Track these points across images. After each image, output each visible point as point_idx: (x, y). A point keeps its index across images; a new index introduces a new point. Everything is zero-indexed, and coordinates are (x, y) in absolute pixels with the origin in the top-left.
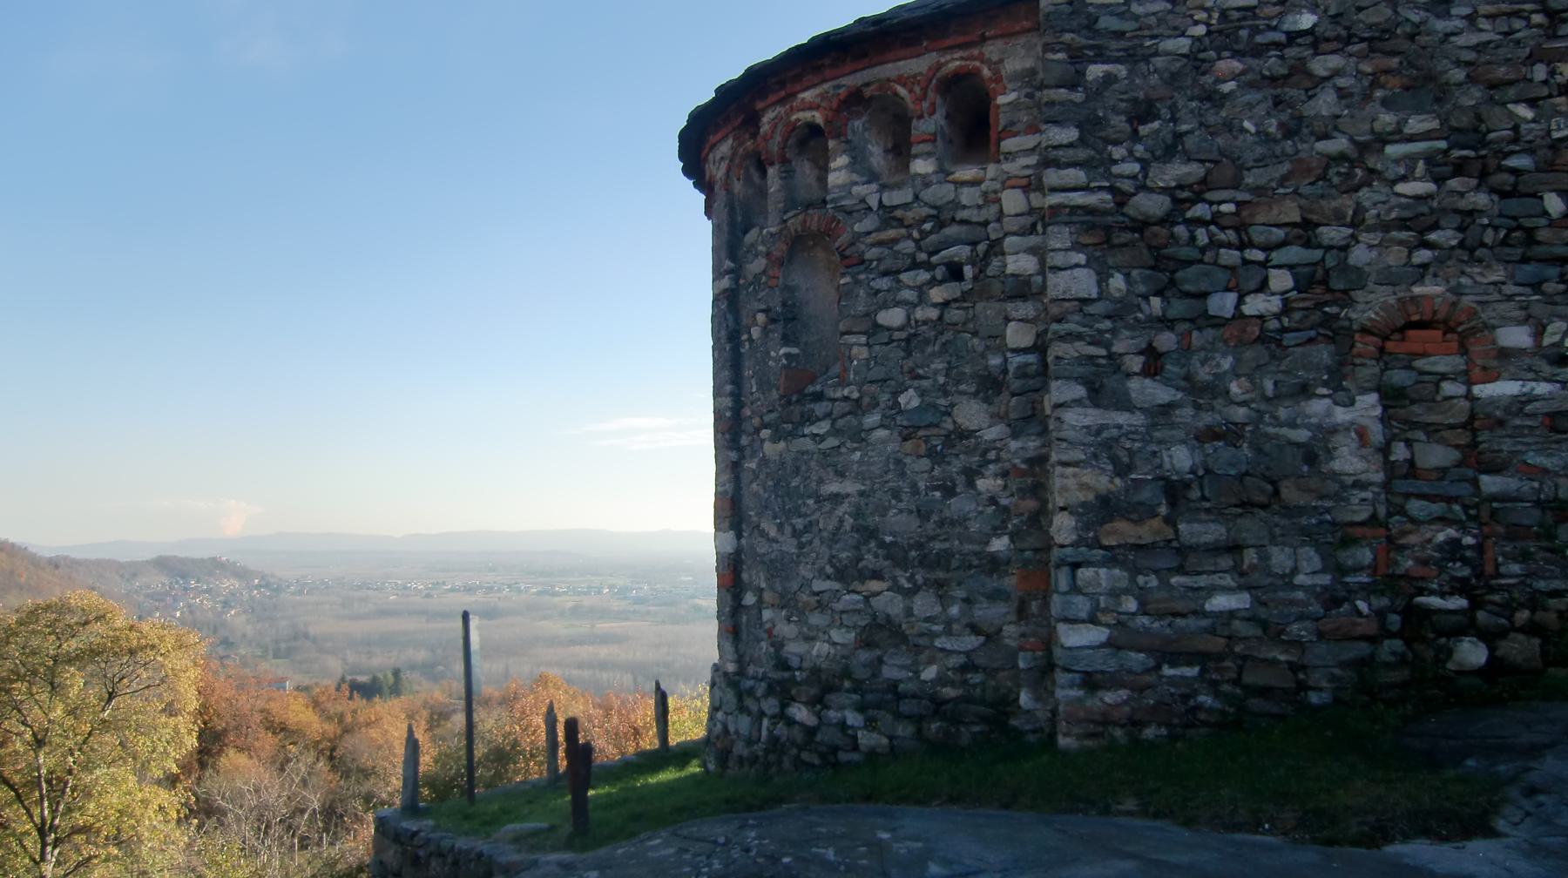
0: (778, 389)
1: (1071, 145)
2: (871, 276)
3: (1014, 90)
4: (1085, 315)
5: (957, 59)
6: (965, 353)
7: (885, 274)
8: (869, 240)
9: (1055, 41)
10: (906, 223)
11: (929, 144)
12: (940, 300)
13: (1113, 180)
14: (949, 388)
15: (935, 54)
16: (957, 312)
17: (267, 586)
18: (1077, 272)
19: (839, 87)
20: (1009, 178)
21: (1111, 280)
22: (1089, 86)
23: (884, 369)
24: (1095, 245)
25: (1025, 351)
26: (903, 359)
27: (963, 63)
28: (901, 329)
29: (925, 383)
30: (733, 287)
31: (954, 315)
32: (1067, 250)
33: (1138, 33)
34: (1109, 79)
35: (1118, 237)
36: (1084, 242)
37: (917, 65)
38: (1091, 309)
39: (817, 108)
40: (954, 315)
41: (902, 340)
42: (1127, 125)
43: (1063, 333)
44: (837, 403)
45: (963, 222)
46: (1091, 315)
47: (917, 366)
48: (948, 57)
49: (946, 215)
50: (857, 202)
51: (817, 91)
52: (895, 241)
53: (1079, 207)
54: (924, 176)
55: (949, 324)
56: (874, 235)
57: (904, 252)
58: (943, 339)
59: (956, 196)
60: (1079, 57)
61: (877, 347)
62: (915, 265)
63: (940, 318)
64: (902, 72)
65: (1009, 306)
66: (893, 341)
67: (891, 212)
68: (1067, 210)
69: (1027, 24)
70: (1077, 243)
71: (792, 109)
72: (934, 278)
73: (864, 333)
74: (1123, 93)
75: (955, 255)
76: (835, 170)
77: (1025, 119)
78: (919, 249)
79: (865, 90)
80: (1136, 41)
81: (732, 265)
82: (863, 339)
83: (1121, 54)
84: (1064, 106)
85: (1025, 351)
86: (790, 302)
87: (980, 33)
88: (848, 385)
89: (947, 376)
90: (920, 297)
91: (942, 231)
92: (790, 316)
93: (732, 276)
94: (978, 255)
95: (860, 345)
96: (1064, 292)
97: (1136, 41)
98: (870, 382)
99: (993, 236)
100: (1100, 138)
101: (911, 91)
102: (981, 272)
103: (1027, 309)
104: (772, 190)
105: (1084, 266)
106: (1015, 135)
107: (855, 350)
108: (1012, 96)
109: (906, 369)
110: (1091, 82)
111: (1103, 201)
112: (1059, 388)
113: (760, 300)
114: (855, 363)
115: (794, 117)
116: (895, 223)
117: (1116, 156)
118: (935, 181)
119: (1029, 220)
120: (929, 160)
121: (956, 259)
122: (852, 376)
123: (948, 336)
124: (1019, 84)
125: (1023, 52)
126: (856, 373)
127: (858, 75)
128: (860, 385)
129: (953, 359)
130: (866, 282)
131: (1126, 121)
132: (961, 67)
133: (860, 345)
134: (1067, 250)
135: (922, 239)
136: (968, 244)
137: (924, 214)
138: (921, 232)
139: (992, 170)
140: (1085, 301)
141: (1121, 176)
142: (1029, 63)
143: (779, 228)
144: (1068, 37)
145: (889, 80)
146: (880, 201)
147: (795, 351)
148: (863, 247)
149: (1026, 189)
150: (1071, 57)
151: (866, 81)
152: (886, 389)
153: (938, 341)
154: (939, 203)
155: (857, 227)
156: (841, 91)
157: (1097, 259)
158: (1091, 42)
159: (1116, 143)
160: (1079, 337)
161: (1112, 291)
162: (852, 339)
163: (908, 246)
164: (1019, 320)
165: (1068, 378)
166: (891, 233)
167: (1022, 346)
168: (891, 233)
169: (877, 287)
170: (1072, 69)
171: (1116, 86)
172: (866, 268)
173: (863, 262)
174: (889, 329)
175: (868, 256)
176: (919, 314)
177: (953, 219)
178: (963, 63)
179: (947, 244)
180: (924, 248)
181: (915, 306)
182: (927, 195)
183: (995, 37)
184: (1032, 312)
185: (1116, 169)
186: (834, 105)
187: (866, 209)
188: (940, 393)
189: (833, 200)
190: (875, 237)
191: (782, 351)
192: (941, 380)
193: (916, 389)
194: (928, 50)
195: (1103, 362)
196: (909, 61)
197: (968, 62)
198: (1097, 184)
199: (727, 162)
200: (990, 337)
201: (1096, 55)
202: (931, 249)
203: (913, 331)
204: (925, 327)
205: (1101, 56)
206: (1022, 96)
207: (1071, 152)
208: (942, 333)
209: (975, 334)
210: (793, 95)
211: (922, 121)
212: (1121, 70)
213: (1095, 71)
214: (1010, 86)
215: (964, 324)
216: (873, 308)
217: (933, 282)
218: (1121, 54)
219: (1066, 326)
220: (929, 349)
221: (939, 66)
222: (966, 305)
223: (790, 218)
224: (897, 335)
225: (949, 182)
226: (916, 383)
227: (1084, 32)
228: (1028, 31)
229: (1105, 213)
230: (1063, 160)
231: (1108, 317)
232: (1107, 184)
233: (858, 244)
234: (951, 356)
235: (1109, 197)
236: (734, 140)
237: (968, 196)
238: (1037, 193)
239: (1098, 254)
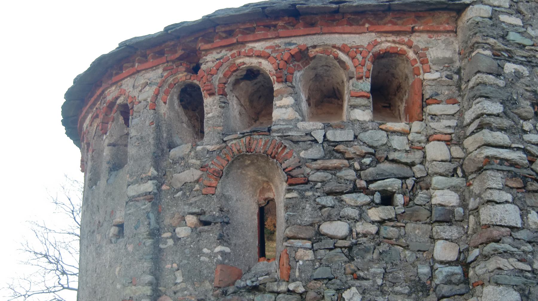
0: (212, 281)
1: (498, 115)
2: (318, 194)
3: (437, 71)
4: (514, 239)
5: (389, 42)
6: (399, 262)
7: (329, 194)
8: (315, 165)
9: (484, 41)
10: (347, 156)
11: (365, 99)
12: (377, 219)
13: (526, 144)
14: (385, 288)
15: (374, 34)
16: (392, 229)
18: (507, 206)
19: (290, 44)
20: (435, 133)
21: (529, 215)
22: (507, 77)
23: (328, 269)
24: (518, 188)
25: (449, 263)
26: (346, 262)
27: (393, 45)
28: (344, 238)
29: (365, 283)
30: (156, 191)
31: (389, 231)
32: (499, 189)
33: (533, 48)
34: (518, 75)
35: (531, 185)
36: (510, 185)
38: (518, 235)
39: (267, 57)
40: (389, 231)
41: (345, 247)
42: (531, 108)
43: (501, 251)
44: (280, 295)
45: (394, 161)
46: (519, 239)
47: (359, 269)
48: (383, 39)
49: (381, 154)
50: (304, 134)
52: (338, 169)
53: (507, 160)
54: (362, 123)
55: (384, 238)
56: (319, 162)
57: (346, 178)
58: (381, 249)
59: (389, 140)
60: (499, 56)
61: (322, 252)
62: (355, 190)
63: (378, 233)
64: (346, 43)
65: (437, 228)
66: (335, 247)
67: (335, 146)
68: (498, 161)
69: (448, 27)
70: (506, 185)
71: (239, 54)
72: (373, 201)
73: (309, 239)
74: (527, 86)
75: (390, 186)
76: (281, 107)
77: (447, 92)
78: (359, 177)
79: (310, 50)
80: (532, 53)
81: (156, 173)
82: (308, 244)
83: (524, 59)
84: (492, 87)
85: (449, 263)
86: (225, 209)
87: (412, 26)
88: (294, 281)
89: (383, 278)
90: (360, 215)
91: (378, 165)
92: (226, 220)
93: (155, 181)
94: (407, 188)
95: (306, 249)
96: (501, 220)
97: (532, 53)
98: (315, 280)
99: (418, 175)
100: (516, 113)
101: (353, 58)
102: (410, 200)
103: (452, 231)
104: (210, 115)
105: (511, 203)
106: (438, 103)
107: (300, 252)
108: (436, 75)
109: (348, 270)
110: (507, 74)
111: (521, 158)
112: (501, 292)
113: (191, 204)
114: (301, 262)
115: (239, 61)
116: (338, 155)
117: (526, 128)
118: (370, 128)
119: (453, 166)
120: (367, 111)
121: (389, 188)
122: (297, 274)
123: (384, 247)
124: (442, 68)
125: (443, 46)
126: (301, 272)
127: (309, 38)
128: (306, 282)
129: (389, 266)
130: (313, 198)
131: (530, 105)
132: (391, 48)
133: (306, 249)
134: (499, 189)
135: (362, 169)
136: (399, 178)
137: (364, 151)
138: (361, 164)
139: (416, 126)
140: (512, 228)
141: (529, 142)
142: (448, 54)
143: (218, 146)
144: (491, 41)
145: (334, 47)
146: (325, 136)
147: (227, 250)
148: (308, 170)
149: (448, 143)
150: (494, 55)
151: (315, 44)
152: (331, 286)
153: (376, 251)
154: (375, 144)
155: (302, 154)
156: (292, 47)
157: (519, 199)
158: (506, 47)
159: (526, 119)
160: (512, 255)
161: (530, 223)
162: (297, 243)
163: (350, 174)
164: (446, 240)
165: (507, 285)
166: (335, 162)
167: (449, 259)
168: (335, 162)
169: (323, 203)
170: (495, 63)
171: (522, 80)
172: (311, 188)
173: (307, 182)
174: (332, 237)
175: (312, 178)
176: (360, 228)
177: (387, 158)
178: (393, 45)
179: (383, 177)
180: (363, 177)
181: (357, 221)
182: (365, 136)
183: (421, 32)
184: (456, 234)
185: (526, 137)
186: (286, 56)
187: (312, 141)
188: (379, 292)
189: (278, 131)
190: (320, 164)
191: (219, 249)
192: (379, 282)
193: (358, 287)
194: (369, 31)
195: (529, 275)
196: (352, 35)
197: (397, 45)
198: (516, 146)
199: (154, 88)
200: (419, 251)
201: (509, 57)
202: (370, 178)
203: (354, 241)
204: (365, 239)
205: (510, 59)
206: (444, 76)
207: (499, 120)
208: (379, 245)
209: (406, 247)
210: (243, 43)
211: (361, 81)
212: (525, 70)
213: (510, 68)
214: (434, 67)
215: (398, 239)
216: (318, 220)
217: (372, 204)
218: (524, 59)
219: (503, 245)
220: (369, 257)
221: (376, 43)
222: (399, 224)
223: (231, 140)
224: (341, 243)
225: (382, 129)
226: (357, 283)
227: (501, 39)
228: (448, 32)
229: (522, 167)
230: (494, 124)
231: (530, 242)
232: (522, 147)
233: (304, 168)
234: (386, 263)
235: (524, 156)
236: (165, 70)
237: (397, 142)
238: (458, 147)
239: (520, 195)
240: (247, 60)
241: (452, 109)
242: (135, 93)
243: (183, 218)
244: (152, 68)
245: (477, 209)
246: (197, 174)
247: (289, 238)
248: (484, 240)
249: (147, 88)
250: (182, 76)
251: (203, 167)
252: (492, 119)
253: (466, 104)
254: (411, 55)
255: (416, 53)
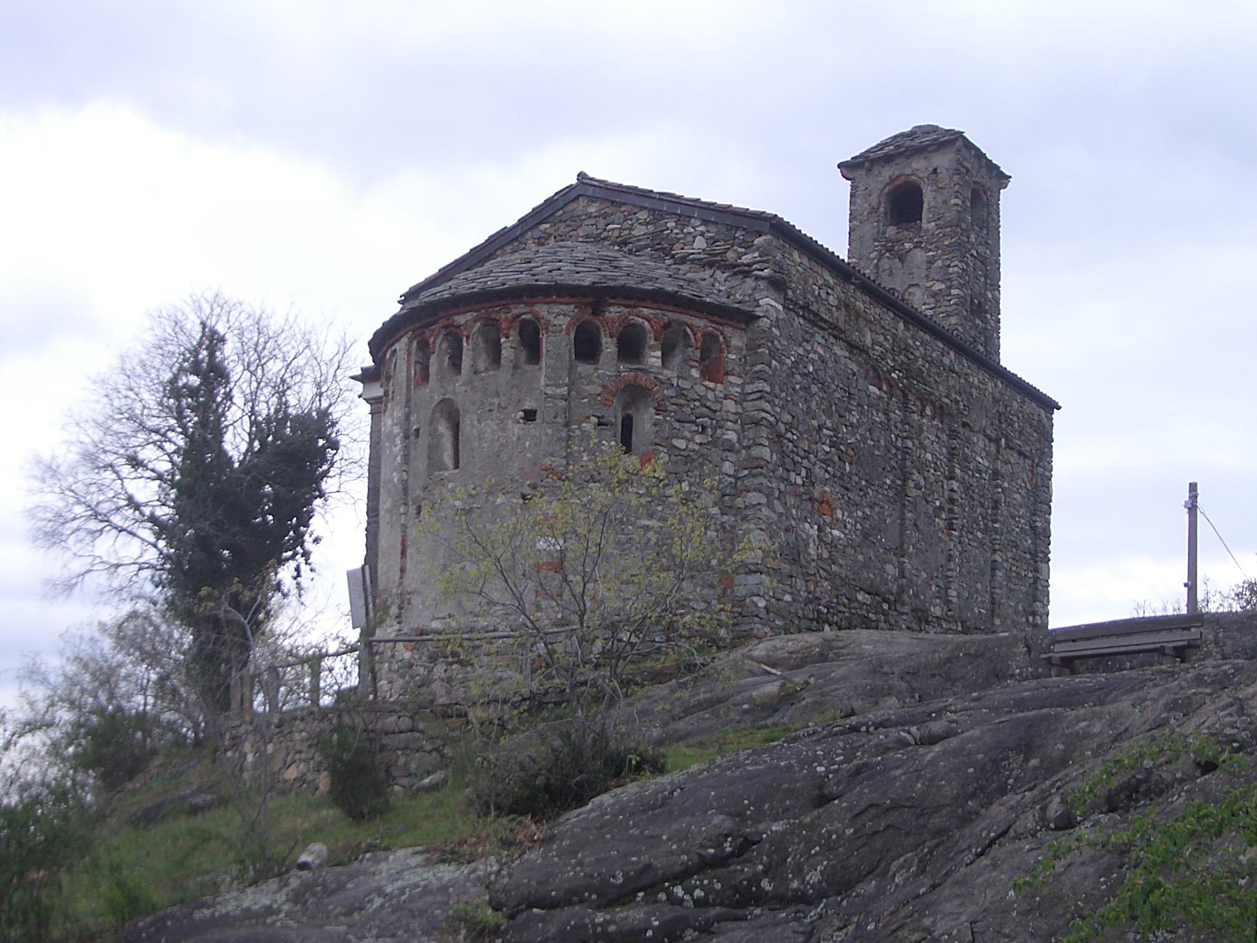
17: (632, 814)
29: (692, 480)
37: (700, 323)
51: (652, 311)
103: (732, 457)
107: (662, 454)
139: (720, 387)
145: (686, 324)
162: (661, 448)
163: (688, 410)
168: (682, 401)
176: (691, 446)
190: (673, 400)
210: (636, 307)
224: (682, 453)
237: (710, 395)
240: (636, 318)
241: (740, 381)
242: (551, 318)
243: (588, 418)
244: (566, 304)
245: (749, 447)
246: (600, 390)
247: (656, 444)
248: (754, 465)
249: (562, 317)
251: (604, 387)
252: (525, 310)
253: (748, 380)
254: (721, 338)
255: (724, 338)
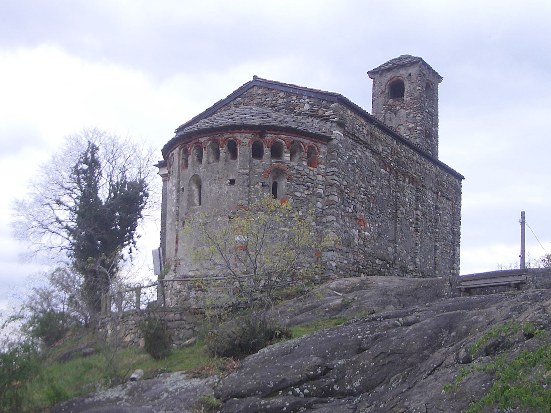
29: (303, 210)
45: (310, 178)
52: (299, 178)
103: (321, 200)
107: (290, 199)
139: (315, 169)
162: (290, 196)
168: (299, 176)
175: (293, 179)
176: (303, 195)
190: (295, 175)
210: (279, 134)
224: (299, 198)
237: (311, 173)
240: (279, 139)
241: (324, 167)
243: (258, 183)
246: (263, 171)
247: (288, 195)
249: (246, 139)
250: (257, 138)
251: (265, 169)
254: (316, 148)
